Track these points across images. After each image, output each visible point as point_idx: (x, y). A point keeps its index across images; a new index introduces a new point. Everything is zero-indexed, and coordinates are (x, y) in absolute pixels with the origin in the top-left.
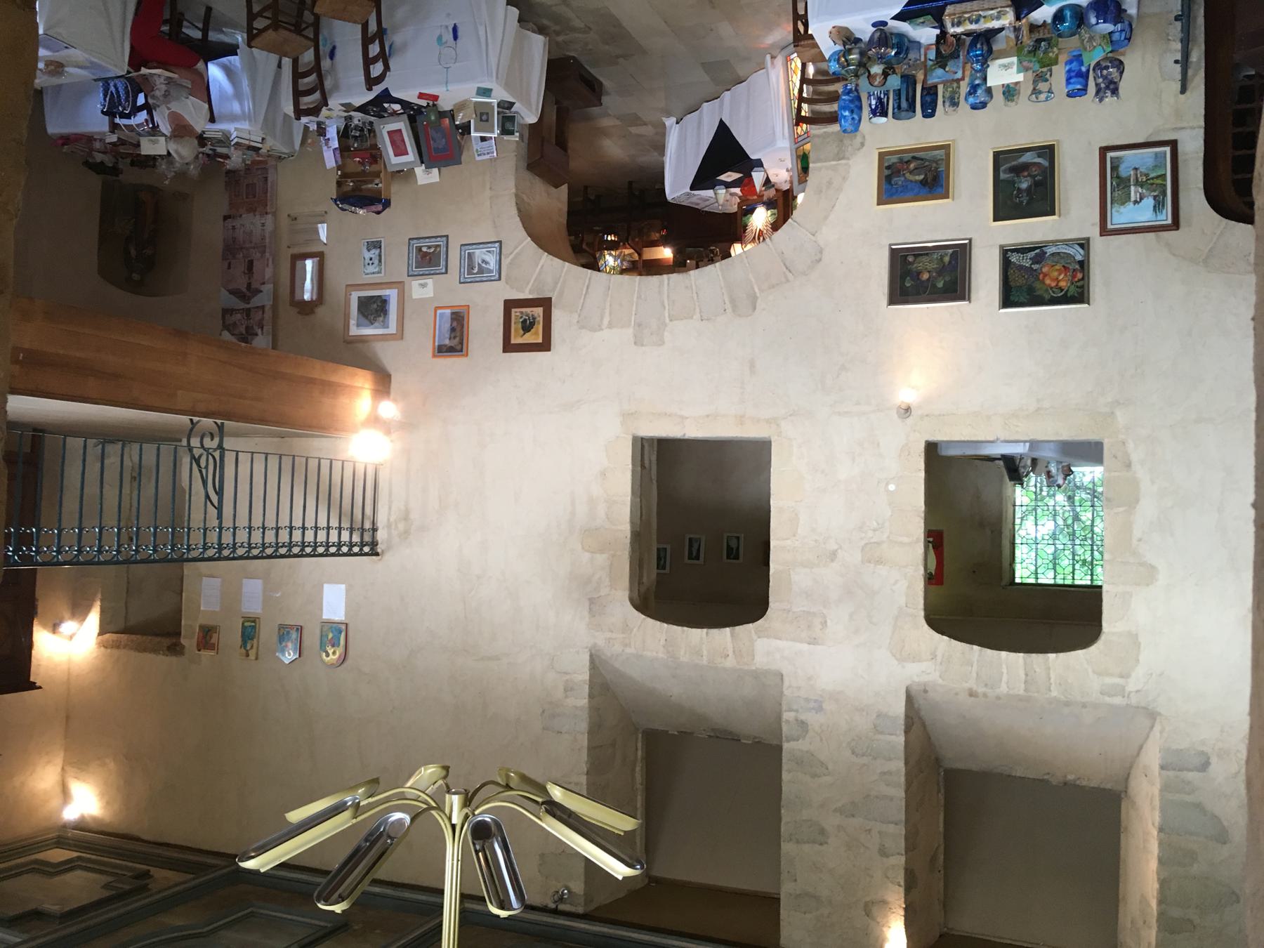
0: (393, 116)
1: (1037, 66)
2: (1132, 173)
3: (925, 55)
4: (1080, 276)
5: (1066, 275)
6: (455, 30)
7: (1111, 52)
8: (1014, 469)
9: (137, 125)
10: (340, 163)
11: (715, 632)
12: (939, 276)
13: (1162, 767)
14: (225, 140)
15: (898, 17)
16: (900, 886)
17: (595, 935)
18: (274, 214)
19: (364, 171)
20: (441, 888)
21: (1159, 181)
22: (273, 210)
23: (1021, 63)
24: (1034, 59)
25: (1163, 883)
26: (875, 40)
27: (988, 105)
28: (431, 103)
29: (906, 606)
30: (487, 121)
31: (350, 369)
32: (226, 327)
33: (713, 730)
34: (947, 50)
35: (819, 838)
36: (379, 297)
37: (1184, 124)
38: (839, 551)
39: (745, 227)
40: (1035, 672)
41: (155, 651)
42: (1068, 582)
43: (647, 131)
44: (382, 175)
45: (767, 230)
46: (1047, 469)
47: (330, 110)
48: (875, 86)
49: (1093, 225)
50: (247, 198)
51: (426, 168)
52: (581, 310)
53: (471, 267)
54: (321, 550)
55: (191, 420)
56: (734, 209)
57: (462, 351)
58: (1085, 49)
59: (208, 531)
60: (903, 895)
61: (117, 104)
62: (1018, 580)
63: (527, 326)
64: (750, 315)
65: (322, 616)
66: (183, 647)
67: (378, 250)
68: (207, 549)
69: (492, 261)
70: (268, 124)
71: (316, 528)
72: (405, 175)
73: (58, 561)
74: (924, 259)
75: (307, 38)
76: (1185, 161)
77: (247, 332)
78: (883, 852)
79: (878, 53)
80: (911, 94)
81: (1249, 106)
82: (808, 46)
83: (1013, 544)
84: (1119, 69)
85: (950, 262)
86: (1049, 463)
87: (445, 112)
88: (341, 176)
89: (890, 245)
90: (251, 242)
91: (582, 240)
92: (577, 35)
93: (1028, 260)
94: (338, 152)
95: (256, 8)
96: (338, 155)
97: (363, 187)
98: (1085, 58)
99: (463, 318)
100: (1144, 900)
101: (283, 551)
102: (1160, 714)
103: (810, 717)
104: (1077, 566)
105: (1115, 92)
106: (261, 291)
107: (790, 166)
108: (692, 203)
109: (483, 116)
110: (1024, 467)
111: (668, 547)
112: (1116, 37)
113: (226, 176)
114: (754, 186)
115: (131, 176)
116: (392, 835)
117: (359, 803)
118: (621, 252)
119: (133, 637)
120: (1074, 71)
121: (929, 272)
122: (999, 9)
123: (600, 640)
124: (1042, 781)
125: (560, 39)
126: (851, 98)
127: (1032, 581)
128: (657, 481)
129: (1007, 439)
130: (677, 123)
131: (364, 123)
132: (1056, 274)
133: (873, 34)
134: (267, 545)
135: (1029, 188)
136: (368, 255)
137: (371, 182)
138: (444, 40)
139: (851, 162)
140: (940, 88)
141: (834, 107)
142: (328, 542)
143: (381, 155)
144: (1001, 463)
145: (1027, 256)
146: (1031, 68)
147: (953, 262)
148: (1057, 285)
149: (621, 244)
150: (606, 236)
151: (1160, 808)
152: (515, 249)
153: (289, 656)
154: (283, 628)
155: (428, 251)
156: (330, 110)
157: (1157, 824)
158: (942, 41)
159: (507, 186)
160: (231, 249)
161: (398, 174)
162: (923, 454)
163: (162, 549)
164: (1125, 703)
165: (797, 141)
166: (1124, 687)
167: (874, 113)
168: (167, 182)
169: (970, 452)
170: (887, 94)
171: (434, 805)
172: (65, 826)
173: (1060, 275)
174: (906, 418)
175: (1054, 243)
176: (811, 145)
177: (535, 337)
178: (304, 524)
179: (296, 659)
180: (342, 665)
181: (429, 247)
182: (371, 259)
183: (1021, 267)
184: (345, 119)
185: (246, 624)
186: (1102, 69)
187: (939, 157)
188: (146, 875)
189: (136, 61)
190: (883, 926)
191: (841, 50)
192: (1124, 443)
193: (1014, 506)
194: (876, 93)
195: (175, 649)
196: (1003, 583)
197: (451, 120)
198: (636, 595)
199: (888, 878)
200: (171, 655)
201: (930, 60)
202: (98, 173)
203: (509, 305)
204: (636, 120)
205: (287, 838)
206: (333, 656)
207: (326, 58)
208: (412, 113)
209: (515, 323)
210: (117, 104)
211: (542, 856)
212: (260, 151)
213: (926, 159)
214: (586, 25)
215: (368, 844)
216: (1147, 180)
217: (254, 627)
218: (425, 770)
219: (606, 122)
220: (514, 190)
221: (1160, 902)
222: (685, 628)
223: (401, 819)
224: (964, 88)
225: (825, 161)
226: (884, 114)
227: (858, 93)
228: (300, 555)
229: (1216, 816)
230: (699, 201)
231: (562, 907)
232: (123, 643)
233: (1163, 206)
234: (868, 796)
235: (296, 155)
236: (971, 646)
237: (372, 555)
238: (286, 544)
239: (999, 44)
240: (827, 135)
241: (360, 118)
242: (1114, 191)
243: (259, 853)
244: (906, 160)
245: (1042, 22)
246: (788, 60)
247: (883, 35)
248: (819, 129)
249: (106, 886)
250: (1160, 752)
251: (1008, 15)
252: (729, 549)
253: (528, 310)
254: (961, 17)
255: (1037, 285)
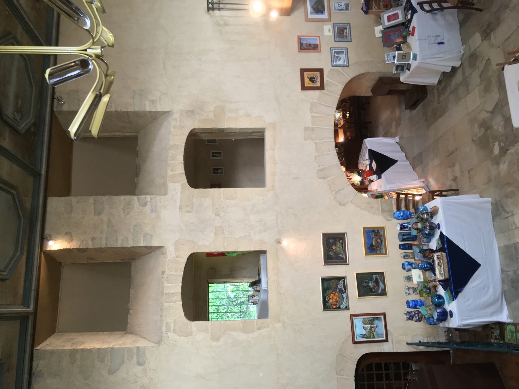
1: (420, 288)
2: (375, 325)
3: (425, 245)
4: (334, 307)
5: (335, 302)
7: (425, 317)
8: (256, 283)
11: (182, 166)
12: (334, 253)
13: (138, 348)
15: (441, 234)
16: (80, 246)
17: (45, 116)
20: (59, 45)
21: (372, 336)
23: (421, 282)
24: (422, 287)
25: (90, 350)
26: (432, 225)
27: (404, 270)
28: (410, 33)
29: (198, 245)
30: (402, 59)
33: (140, 166)
34: (427, 253)
35: (98, 213)
36: (324, 10)
37: (394, 345)
38: (220, 217)
39: (353, 172)
40: (174, 297)
42: (210, 304)
43: (393, 130)
44: (379, 10)
45: (351, 182)
46: (255, 296)
48: (413, 225)
49: (355, 312)
51: (382, 31)
52: (319, 103)
53: (338, 53)
56: (360, 167)
58: (426, 307)
60: (76, 247)
62: (210, 285)
63: (312, 79)
64: (318, 177)
67: (345, 9)
69: (340, 62)
72: (378, 21)
74: (341, 247)
76: (380, 345)
78: (93, 239)
79: (427, 226)
80: (409, 239)
81: (401, 368)
82: (429, 197)
83: (224, 283)
84: (418, 320)
85: (340, 257)
86: (258, 296)
87: (406, 39)
89: (347, 233)
91: (346, 102)
93: (340, 287)
98: (423, 307)
99: (315, 50)
100: (83, 343)
102: (159, 345)
103: (147, 209)
104: (217, 307)
105: (409, 319)
107: (378, 190)
108: (363, 150)
109: (404, 57)
110: (256, 287)
111: (217, 144)
112: (431, 319)
114: (370, 176)
116: (79, 20)
117: (93, 3)
118: (341, 120)
120: (417, 303)
121: (336, 249)
122: (444, 274)
123: (176, 116)
124: (129, 301)
125: (435, 91)
126: (408, 215)
127: (210, 291)
128: (246, 139)
129: (268, 282)
130: (396, 142)
132: (335, 298)
133: (435, 224)
135: (369, 286)
136: (343, 4)
137: (376, 5)
138: (438, 38)
139: (381, 216)
140: (411, 251)
141: (403, 209)
143: (388, 10)
144: (257, 279)
145: (342, 287)
146: (419, 286)
147: (340, 258)
148: (330, 298)
149: (345, 120)
150: (349, 113)
151: (121, 348)
152: (345, 73)
155: (345, 33)
157: (114, 347)
158: (431, 251)
159: (373, 69)
162: (261, 250)
164: (163, 332)
165: (388, 193)
166: (170, 331)
167: (402, 225)
169: (262, 267)
170: (409, 230)
171: (95, 40)
173: (335, 299)
174: (276, 243)
175: (347, 297)
176: (387, 199)
177: (308, 83)
181: (346, 33)
182: (341, 5)
183: (337, 285)
186: (418, 314)
187: (382, 251)
190: (62, 240)
191: (428, 211)
192: (268, 327)
193: (240, 283)
194: (410, 225)
196: (208, 280)
197: (403, 42)
198: (196, 131)
199: (83, 241)
201: (423, 247)
203: (321, 71)
204: (398, 124)
208: (406, 24)
209: (313, 74)
211: (77, 91)
213: (381, 245)
214: (441, 102)
215: (74, 9)
216: (372, 331)
218: (111, 36)
219: (397, 112)
221: (82, 350)
222: (183, 153)
224: (411, 260)
225: (381, 205)
226: (401, 229)
227: (410, 218)
229: (119, 369)
230: (363, 153)
231: (55, 101)
233: (362, 338)
234: (117, 232)
236: (183, 271)
239: (429, 274)
240: (391, 204)
242: (368, 319)
244: (381, 237)
245: (437, 290)
246: (421, 188)
247: (434, 228)
248: (394, 203)
250: (144, 346)
251: (441, 277)
252: (217, 170)
254: (441, 259)
255: (331, 291)
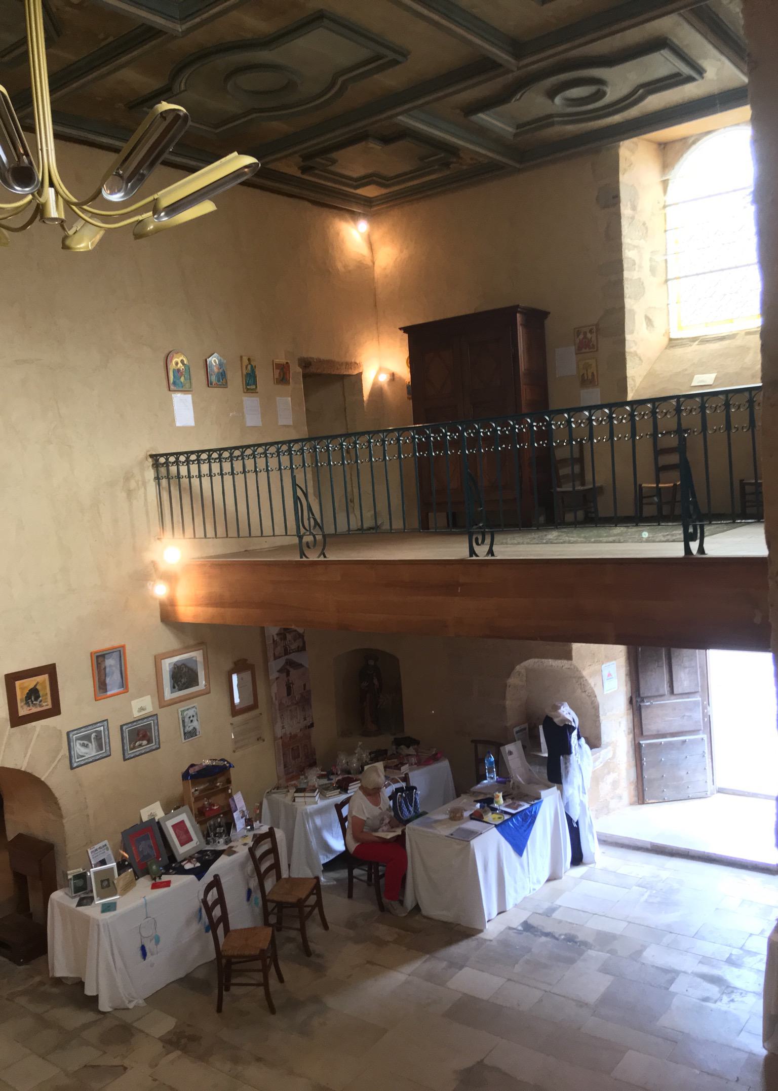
0: (190, 857)
6: (144, 954)
9: (389, 785)
10: (230, 800)
14: (324, 791)
18: (275, 739)
19: (208, 798)
22: (276, 742)
28: (158, 880)
30: (102, 881)
31: (199, 621)
32: (301, 636)
36: (180, 690)
41: (320, 361)
44: (193, 800)
47: (245, 844)
50: (298, 746)
53: (98, 738)
54: (204, 456)
55: (325, 557)
57: (97, 657)
59: (302, 465)
61: (407, 798)
63: (33, 694)
65: (192, 397)
66: (300, 365)
67: (186, 731)
68: (300, 450)
69: (79, 749)
70: (292, 814)
71: (211, 476)
73: (399, 431)
75: (273, 901)
77: (285, 635)
88: (228, 788)
90: (290, 710)
92: (20, 988)
94: (233, 809)
95: (316, 911)
96: (232, 806)
97: (208, 784)
101: (237, 453)
106: (278, 671)
113: (316, 759)
115: (385, 741)
116: (118, 178)
119: (337, 372)
125: (38, 979)
131: (214, 841)
134: (252, 457)
136: (195, 724)
137: (202, 791)
142: (199, 463)
143: (196, 817)
152: (56, 765)
153: (214, 360)
154: (224, 385)
155: (141, 742)
156: (245, 844)
160: (305, 701)
161: (178, 805)
163: (336, 447)
168: (360, 743)
172: (365, 215)
178: (222, 478)
179: (209, 357)
180: (167, 352)
181: (140, 745)
182: (192, 721)
184: (230, 839)
185: (254, 387)
188: (305, 170)
189: (401, 839)
195: (305, 364)
200: (307, 358)
202: (409, 737)
203: (55, 710)
205: (190, 198)
206: (177, 361)
207: (254, 888)
208: (173, 865)
209: (47, 694)
210: (407, 798)
212: (295, 790)
217: (247, 384)
220: (64, 821)
223: (111, 194)
228: (231, 449)
232: (344, 367)
235: (265, 794)
237: (156, 455)
238: (235, 459)
241: (218, 845)
243: (241, 171)
249: (334, 162)
253: (34, 710)
